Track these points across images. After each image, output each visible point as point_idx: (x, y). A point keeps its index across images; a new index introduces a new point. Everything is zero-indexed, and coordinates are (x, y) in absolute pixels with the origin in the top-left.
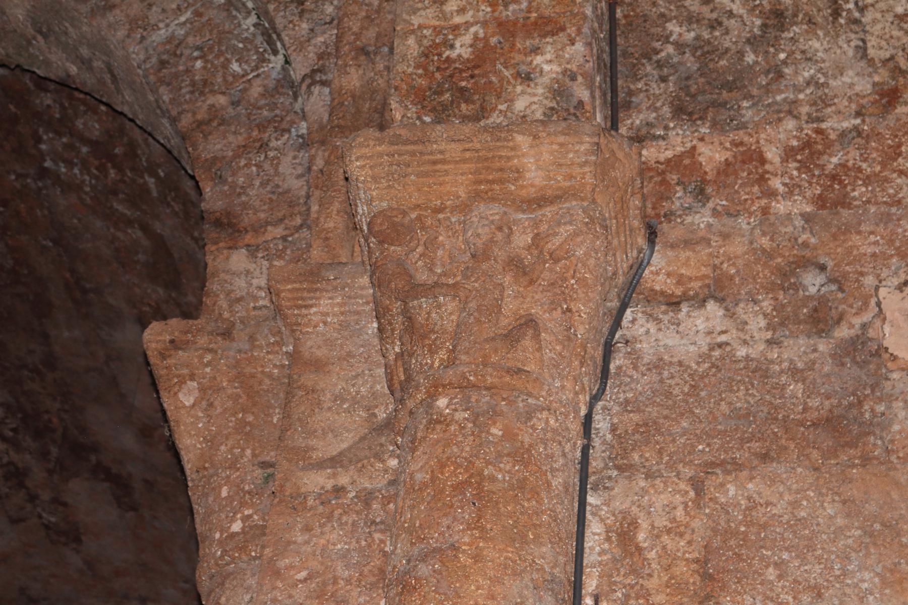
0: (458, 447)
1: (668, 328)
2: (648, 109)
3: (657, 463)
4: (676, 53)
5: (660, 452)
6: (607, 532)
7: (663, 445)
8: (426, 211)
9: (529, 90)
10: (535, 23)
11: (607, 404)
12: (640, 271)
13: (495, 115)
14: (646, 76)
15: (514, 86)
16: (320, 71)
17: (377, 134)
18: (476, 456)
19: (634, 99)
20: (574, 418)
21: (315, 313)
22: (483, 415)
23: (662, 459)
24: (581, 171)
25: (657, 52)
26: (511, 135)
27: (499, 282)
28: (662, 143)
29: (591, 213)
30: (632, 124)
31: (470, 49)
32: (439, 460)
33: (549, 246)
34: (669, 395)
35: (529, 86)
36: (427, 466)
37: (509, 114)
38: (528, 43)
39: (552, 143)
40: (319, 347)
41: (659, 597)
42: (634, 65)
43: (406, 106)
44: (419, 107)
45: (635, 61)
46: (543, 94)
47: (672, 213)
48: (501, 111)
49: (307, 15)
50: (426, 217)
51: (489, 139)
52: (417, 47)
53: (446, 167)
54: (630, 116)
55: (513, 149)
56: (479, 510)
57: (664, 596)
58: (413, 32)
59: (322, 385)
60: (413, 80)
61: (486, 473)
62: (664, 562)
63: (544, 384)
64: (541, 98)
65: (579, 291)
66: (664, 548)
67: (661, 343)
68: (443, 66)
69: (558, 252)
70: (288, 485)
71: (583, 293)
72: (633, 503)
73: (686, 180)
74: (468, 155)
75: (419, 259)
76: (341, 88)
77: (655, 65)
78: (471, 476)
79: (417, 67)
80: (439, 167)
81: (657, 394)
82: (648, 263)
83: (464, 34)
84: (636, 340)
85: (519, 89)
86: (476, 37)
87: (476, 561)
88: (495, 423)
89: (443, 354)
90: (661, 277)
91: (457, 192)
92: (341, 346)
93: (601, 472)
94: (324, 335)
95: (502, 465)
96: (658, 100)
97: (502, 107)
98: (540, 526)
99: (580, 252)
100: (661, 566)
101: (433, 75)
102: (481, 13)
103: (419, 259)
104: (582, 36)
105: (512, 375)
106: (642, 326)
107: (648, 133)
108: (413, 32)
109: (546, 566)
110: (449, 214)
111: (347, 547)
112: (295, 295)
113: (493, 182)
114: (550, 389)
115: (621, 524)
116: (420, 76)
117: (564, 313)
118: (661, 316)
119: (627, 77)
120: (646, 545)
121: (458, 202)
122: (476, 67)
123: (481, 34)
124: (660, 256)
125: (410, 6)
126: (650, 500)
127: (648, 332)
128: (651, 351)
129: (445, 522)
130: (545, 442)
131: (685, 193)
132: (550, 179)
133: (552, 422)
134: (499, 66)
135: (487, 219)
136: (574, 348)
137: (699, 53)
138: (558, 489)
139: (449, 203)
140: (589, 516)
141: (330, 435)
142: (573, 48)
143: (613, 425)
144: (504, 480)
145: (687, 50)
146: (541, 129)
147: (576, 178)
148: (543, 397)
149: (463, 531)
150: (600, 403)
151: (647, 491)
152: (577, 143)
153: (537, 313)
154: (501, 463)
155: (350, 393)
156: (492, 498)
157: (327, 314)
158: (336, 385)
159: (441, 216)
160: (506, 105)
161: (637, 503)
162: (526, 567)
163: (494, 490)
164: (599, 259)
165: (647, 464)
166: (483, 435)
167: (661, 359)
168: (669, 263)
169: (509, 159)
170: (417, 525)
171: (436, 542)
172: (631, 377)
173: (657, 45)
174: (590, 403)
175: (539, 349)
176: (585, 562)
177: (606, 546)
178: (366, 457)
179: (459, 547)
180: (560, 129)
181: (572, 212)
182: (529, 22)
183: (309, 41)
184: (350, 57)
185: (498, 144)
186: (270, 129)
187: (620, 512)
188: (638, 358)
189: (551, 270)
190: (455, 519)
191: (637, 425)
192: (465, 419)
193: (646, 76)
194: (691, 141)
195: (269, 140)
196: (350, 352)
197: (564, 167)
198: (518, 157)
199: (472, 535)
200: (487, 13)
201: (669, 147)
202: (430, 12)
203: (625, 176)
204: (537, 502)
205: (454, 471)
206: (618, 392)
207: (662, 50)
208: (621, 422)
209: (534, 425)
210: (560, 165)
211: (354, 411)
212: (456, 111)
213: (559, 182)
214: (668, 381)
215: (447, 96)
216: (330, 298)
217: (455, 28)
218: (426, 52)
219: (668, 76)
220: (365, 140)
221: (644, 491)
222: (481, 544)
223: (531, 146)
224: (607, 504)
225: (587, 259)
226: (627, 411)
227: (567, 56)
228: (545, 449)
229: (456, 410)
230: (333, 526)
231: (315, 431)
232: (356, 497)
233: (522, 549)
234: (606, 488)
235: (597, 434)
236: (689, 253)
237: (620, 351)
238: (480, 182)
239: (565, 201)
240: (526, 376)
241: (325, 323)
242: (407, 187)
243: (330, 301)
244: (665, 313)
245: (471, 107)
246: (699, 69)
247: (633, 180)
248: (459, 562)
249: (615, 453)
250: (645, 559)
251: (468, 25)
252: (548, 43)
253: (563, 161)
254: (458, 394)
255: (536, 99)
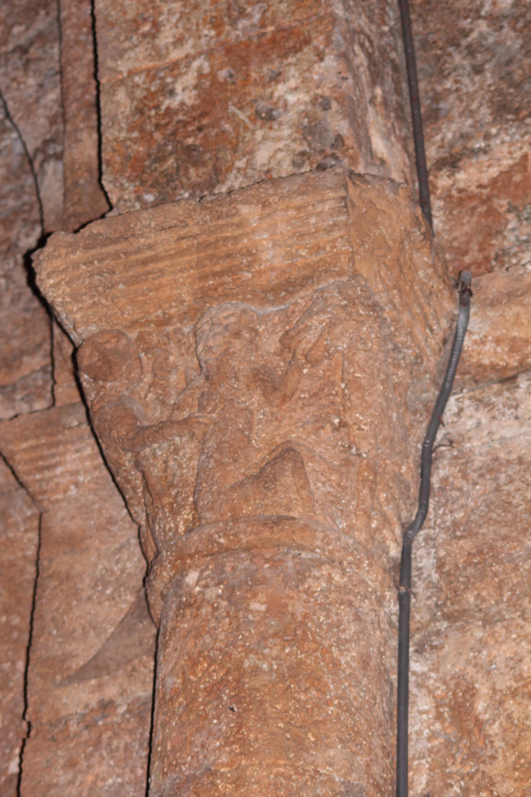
0: (211, 636)
1: (504, 415)
2: (461, 114)
3: (497, 603)
4: (490, 30)
5: (500, 587)
6: (437, 707)
7: (502, 577)
8: (148, 326)
9: (272, 134)
10: (273, 41)
11: (432, 532)
12: (458, 344)
13: (232, 176)
14: (455, 69)
15: (253, 132)
16: (52, 140)
17: (70, 238)
18: (232, 644)
19: (442, 105)
20: (370, 565)
21: (62, 474)
22: (240, 588)
23: (502, 595)
24: (330, 238)
25: (466, 33)
26: (235, 208)
27: (242, 406)
28: (483, 158)
29: (350, 292)
30: (442, 140)
31: (194, 92)
32: (190, 658)
33: (303, 345)
34: (506, 507)
35: (271, 128)
36: (178, 668)
37: (250, 172)
38: (265, 70)
39: (288, 208)
40: (73, 518)
41: (505, 786)
42: (438, 58)
43: (122, 185)
44: (138, 183)
45: (439, 52)
46: (290, 136)
47: (505, 252)
48: (239, 170)
49: (33, 67)
50: (150, 334)
51: (208, 217)
52: (128, 101)
53: (160, 265)
54: (440, 130)
55: (239, 225)
56: (239, 716)
57: (512, 783)
58: (122, 82)
59: (78, 568)
60: (127, 147)
61: (247, 664)
62: (511, 736)
63: (316, 531)
64: (287, 142)
65: (352, 397)
66: (509, 717)
67: (497, 437)
68: (163, 122)
69: (313, 352)
70: (44, 709)
71: (358, 398)
72: (468, 662)
73: (518, 203)
74: (184, 244)
75: (149, 391)
76: (73, 162)
77: (466, 52)
78: (227, 674)
79: (130, 130)
80: (151, 267)
81: (492, 507)
82: (465, 330)
83: (186, 73)
84: (463, 438)
85: (259, 134)
86: (201, 75)
87: (237, 787)
88: (255, 595)
89: (187, 514)
90: (489, 347)
91: (180, 295)
92: (100, 511)
93: (427, 626)
94: (77, 500)
95: (267, 651)
96: (473, 100)
97: (240, 164)
98: (324, 722)
99: (343, 346)
100: (507, 743)
101: (152, 137)
102: (203, 41)
103: (149, 391)
104: (332, 46)
105: (272, 528)
106: (471, 417)
107: (465, 148)
108: (122, 82)
109: (335, 775)
110: (178, 325)
111: (119, 780)
112: (33, 455)
113: (222, 273)
114: (326, 536)
115: (455, 694)
116: (135, 141)
117: (336, 429)
118: (494, 399)
119: (431, 76)
120: (487, 716)
121: (184, 308)
122: (204, 114)
123: (207, 69)
124: (479, 320)
125: (114, 48)
126: (489, 655)
127: (479, 424)
128: (484, 450)
129: (199, 739)
130: (326, 608)
131: (520, 221)
132: (293, 256)
133: (337, 577)
134: (232, 109)
135: (220, 324)
136: (359, 473)
137: (520, 25)
138: (350, 666)
139: (173, 311)
140: (413, 689)
141: (92, 633)
142: (323, 64)
143: (439, 559)
144: (271, 669)
145: (505, 24)
146: (271, 191)
147: (324, 249)
148: (318, 547)
149: (220, 748)
150: (422, 533)
151: (486, 643)
152: (319, 202)
153: (299, 437)
154: (265, 647)
155: (113, 573)
156: (255, 698)
157: (76, 473)
158: (96, 565)
159: (169, 329)
160: (244, 160)
161: (473, 662)
162: (307, 781)
163: (257, 686)
164: (370, 350)
165: (484, 606)
166: (241, 614)
167: (496, 459)
168: (495, 326)
169: (236, 239)
170: (169, 748)
171: (189, 769)
172: (460, 489)
173: (466, 24)
174: (405, 535)
175: (306, 485)
176: (411, 753)
177: (438, 726)
178: (137, 656)
179: (217, 771)
180: (296, 187)
181: (325, 295)
182: (264, 40)
183: (37, 101)
184: (80, 118)
185: (221, 222)
186: (19, 223)
187: (453, 678)
188: (467, 462)
189: (310, 376)
190: (210, 733)
191: (469, 554)
192: (219, 596)
193: (455, 69)
194: (521, 148)
195: (18, 239)
196: (111, 517)
197: (307, 237)
198: (247, 234)
199: (232, 751)
200: (211, 38)
201: (492, 162)
202: (141, 52)
203: (394, 230)
204: (318, 690)
205: (208, 669)
206: (444, 514)
207: (472, 30)
208: (448, 554)
209: (309, 587)
210: (302, 236)
211: (120, 596)
212: (184, 180)
213: (304, 257)
214: (506, 488)
215: (171, 162)
216: (77, 451)
217: (175, 65)
218: (141, 106)
219: (483, 65)
220: (55, 250)
221: (483, 643)
222: (243, 762)
223: (262, 218)
224: (435, 669)
225: (354, 354)
226: (456, 537)
227: (316, 77)
228: (328, 616)
229: (206, 586)
230: (101, 755)
231: (73, 632)
232: (128, 711)
233: (298, 758)
234: (433, 647)
235: (419, 576)
236: (516, 309)
237: (444, 457)
238: (204, 277)
239: (319, 281)
240: (291, 525)
241: (77, 484)
242: (116, 301)
243: (78, 455)
244: (499, 394)
245: (202, 170)
246: (522, 47)
247: (408, 234)
248: (217, 790)
249: (443, 596)
250: (486, 736)
251: (189, 58)
252: (290, 64)
253: (304, 229)
254: (209, 563)
255: (281, 145)
